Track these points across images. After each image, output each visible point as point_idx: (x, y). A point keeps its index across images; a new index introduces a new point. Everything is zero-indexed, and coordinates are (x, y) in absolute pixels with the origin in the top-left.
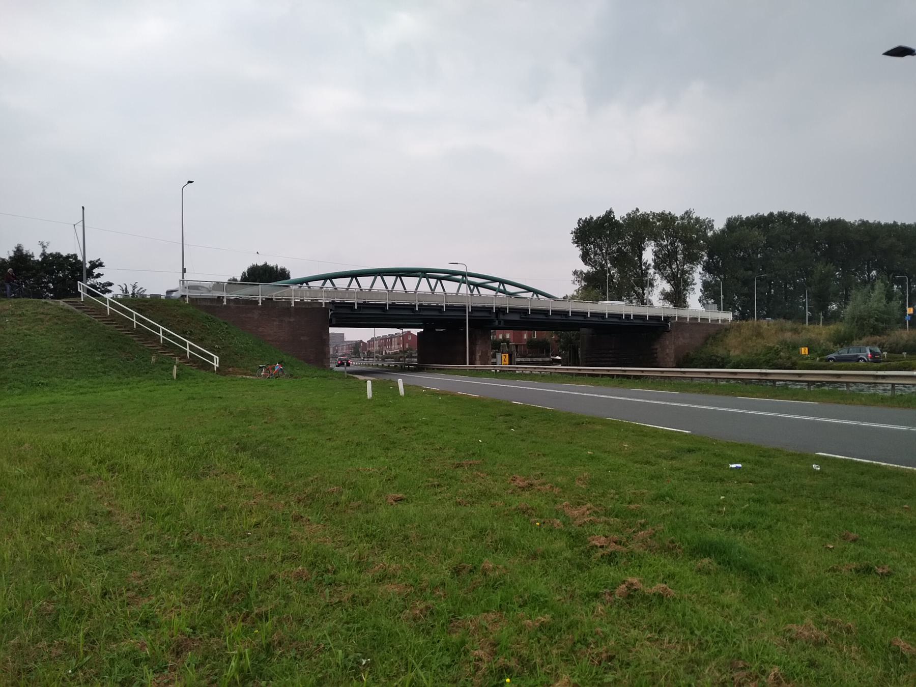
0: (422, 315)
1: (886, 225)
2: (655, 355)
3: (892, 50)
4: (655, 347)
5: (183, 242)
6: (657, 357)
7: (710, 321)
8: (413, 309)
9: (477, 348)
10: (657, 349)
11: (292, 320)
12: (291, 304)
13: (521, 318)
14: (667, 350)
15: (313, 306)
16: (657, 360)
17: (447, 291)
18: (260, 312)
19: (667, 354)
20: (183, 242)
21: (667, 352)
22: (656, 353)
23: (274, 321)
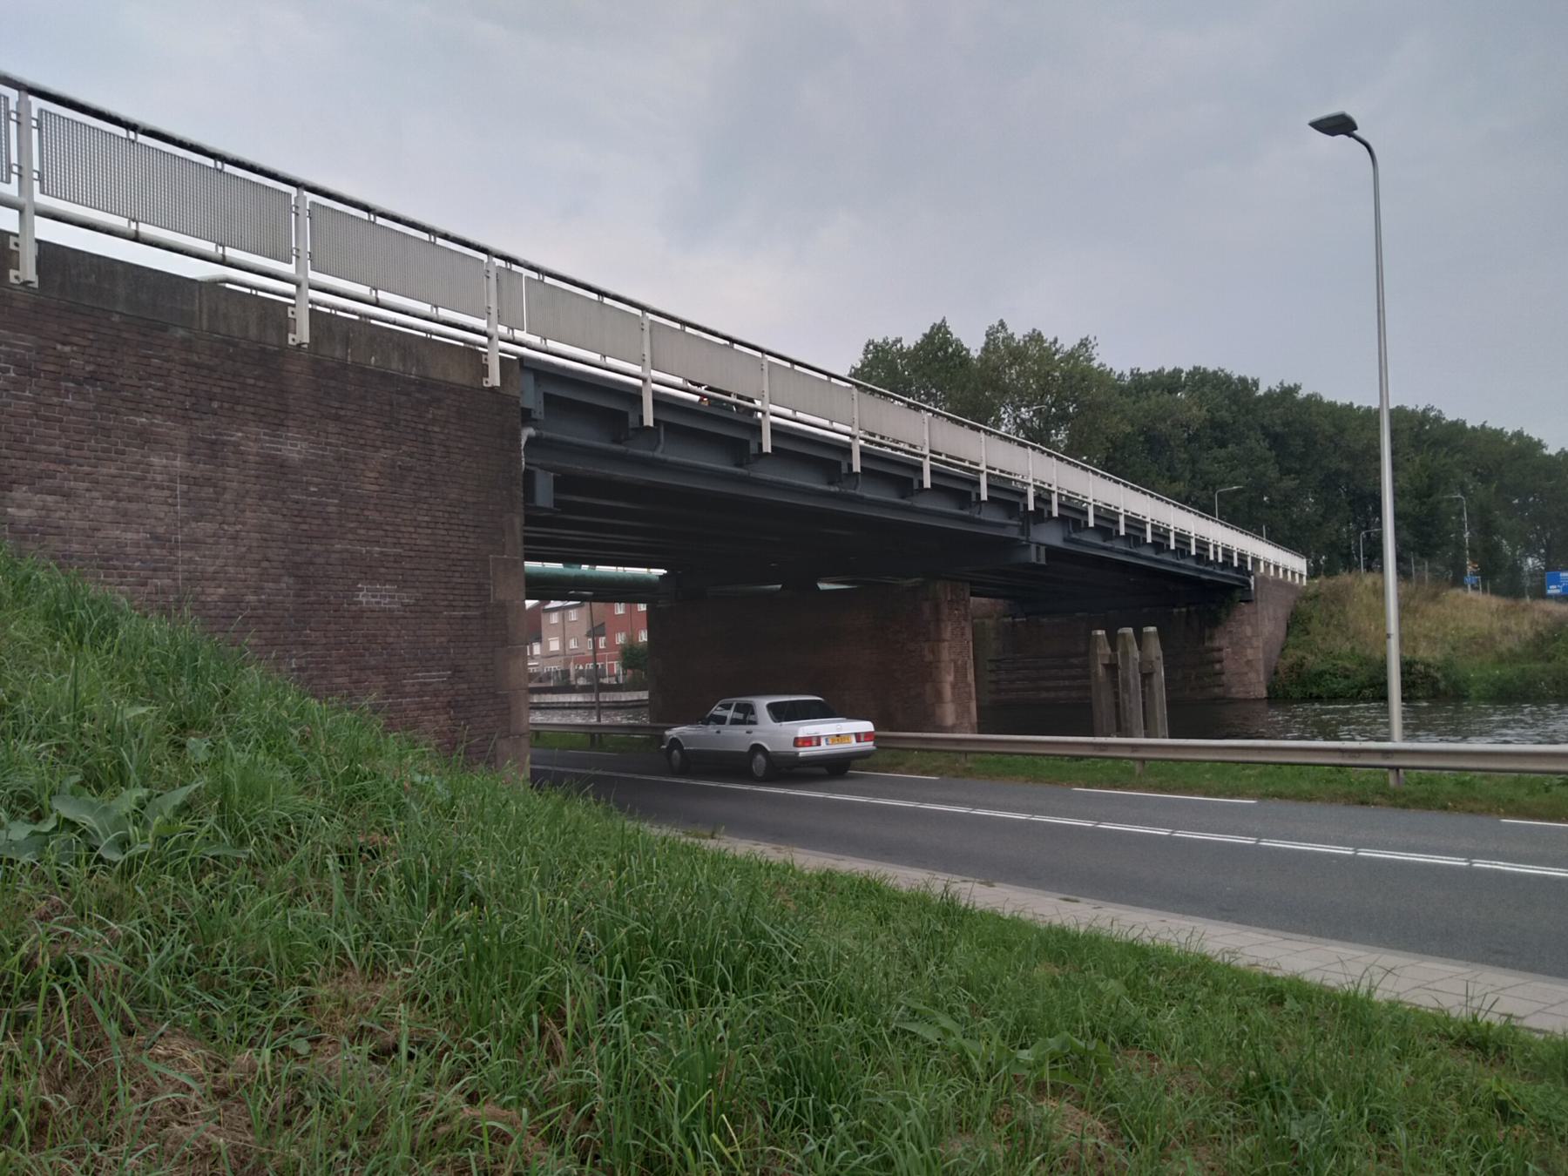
0: (861, 500)
1: (1332, 405)
2: (1218, 666)
3: (1329, 119)
4: (1217, 644)
5: (1380, 312)
6: (1221, 673)
7: (494, 379)
8: (621, 417)
9: (945, 655)
10: (1220, 650)
11: (294, 449)
12: (484, 370)
13: (1065, 540)
14: (1249, 651)
15: (436, 373)
16: (1224, 678)
17: (844, 373)
18: (24, 343)
19: (1248, 662)
20: (1380, 312)
21: (1250, 658)
22: (1220, 661)
23: (145, 438)
